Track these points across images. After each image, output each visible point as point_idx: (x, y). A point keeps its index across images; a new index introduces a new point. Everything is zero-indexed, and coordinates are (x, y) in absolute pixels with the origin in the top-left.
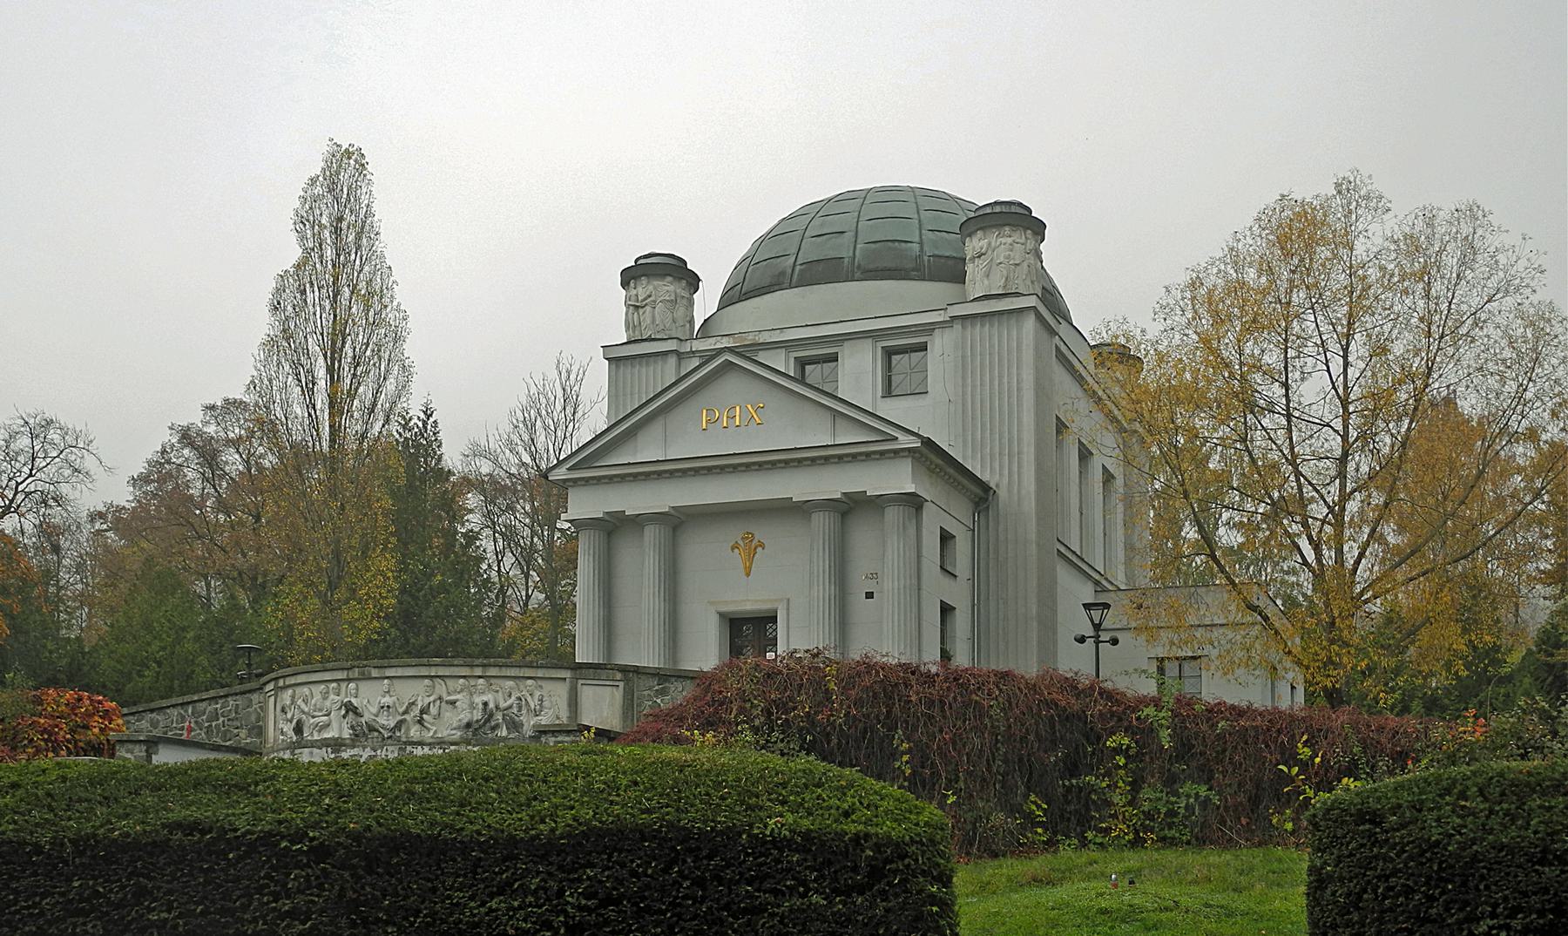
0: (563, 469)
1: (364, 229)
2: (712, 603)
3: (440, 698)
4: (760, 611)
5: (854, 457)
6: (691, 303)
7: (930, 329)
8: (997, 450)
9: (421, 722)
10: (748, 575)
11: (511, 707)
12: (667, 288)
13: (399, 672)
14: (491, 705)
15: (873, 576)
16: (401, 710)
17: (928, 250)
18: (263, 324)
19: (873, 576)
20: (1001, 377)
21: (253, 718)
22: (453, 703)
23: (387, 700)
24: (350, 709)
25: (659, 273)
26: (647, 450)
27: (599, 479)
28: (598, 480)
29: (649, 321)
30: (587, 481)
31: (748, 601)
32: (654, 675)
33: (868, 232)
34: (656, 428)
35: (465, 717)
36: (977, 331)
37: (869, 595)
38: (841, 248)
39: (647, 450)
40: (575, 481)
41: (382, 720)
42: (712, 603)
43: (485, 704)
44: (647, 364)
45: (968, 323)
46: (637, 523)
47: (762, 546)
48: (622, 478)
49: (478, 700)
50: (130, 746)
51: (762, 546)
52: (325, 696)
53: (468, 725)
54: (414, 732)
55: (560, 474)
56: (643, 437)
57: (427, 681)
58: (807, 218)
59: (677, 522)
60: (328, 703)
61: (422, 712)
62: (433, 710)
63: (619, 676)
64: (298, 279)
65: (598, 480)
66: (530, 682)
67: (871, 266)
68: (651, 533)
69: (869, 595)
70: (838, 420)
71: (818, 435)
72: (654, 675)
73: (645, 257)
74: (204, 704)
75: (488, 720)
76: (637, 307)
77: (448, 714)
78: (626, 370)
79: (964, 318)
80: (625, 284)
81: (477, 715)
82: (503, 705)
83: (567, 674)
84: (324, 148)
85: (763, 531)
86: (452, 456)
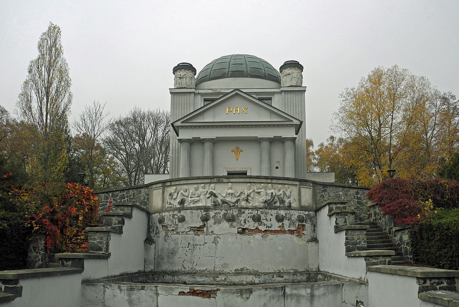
1: (59, 53)
3: (254, 191)
4: (241, 171)
5: (278, 126)
7: (273, 93)
9: (247, 200)
10: (237, 160)
11: (280, 195)
13: (237, 180)
14: (274, 194)
15: (278, 162)
16: (237, 195)
17: (267, 73)
18: (25, 76)
19: (278, 162)
20: (296, 109)
21: (142, 198)
22: (259, 193)
23: (230, 191)
24: (212, 194)
26: (208, 118)
27: (191, 126)
29: (185, 82)
30: (187, 127)
32: (321, 185)
33: (250, 65)
34: (211, 112)
35: (264, 198)
36: (289, 96)
37: (277, 168)
38: (243, 68)
39: (208, 118)
40: (182, 127)
41: (228, 199)
43: (272, 193)
44: (184, 96)
45: (286, 93)
47: (242, 151)
49: (269, 192)
50: (122, 208)
51: (242, 151)
52: (197, 189)
53: (265, 202)
54: (243, 204)
55: (179, 124)
56: (206, 115)
57: (249, 184)
59: (215, 142)
60: (198, 192)
61: (248, 196)
62: (252, 195)
63: (311, 185)
64: (37, 64)
66: (286, 186)
67: (252, 74)
69: (277, 168)
70: (272, 114)
71: (265, 117)
72: (321, 185)
73: (183, 63)
74: (117, 193)
75: (273, 200)
76: (180, 78)
77: (257, 197)
78: (177, 97)
79: (285, 91)
80: (174, 73)
81: (269, 198)
82: (278, 194)
83: (297, 183)
84: (48, 25)
85: (242, 146)
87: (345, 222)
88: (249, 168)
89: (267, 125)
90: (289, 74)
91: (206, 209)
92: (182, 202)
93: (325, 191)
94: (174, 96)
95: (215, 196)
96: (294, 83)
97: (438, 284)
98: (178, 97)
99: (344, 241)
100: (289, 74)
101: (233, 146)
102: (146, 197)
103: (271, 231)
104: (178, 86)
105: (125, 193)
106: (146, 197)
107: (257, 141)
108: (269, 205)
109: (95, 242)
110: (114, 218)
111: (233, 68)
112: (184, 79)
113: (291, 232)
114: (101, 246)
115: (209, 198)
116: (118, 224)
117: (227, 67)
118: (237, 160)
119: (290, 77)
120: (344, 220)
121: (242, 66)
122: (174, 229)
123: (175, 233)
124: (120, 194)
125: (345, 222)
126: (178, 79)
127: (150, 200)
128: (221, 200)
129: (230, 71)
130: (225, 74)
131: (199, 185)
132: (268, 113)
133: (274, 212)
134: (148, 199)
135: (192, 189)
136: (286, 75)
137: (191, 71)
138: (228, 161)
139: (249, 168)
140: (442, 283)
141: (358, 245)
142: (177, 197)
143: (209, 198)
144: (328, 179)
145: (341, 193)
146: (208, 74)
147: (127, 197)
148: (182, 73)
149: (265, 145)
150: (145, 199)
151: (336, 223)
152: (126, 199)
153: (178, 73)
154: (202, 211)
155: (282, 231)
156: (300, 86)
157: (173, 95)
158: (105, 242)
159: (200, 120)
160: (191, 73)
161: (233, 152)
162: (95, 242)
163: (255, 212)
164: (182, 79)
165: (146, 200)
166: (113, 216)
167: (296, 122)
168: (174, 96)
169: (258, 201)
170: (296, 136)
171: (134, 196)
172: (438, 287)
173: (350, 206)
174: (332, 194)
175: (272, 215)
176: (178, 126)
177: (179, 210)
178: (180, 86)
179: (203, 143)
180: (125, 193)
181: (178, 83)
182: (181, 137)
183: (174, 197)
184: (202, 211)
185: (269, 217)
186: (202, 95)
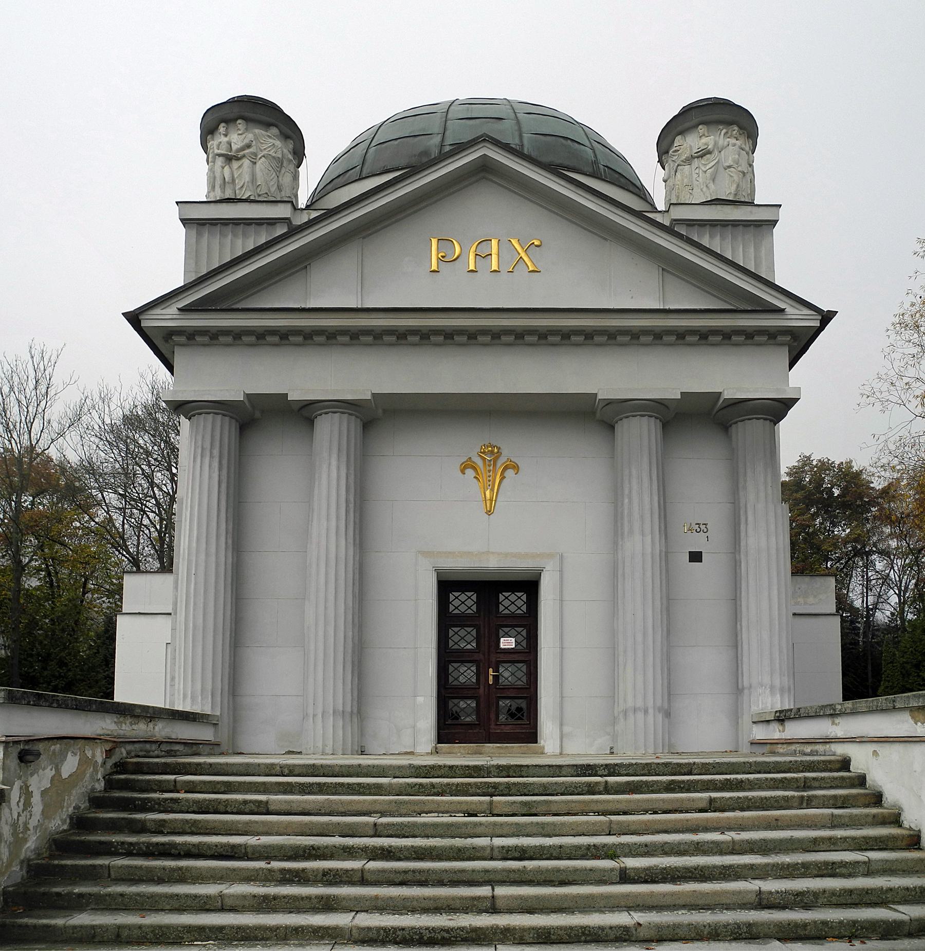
0: (172, 310)
2: (426, 554)
6: (296, 177)
8: (632, 863)
10: (489, 513)
12: (270, 143)
15: (701, 528)
25: (247, 119)
26: (333, 289)
28: (237, 336)
29: (247, 178)
30: (214, 337)
31: (490, 548)
37: (696, 557)
42: (426, 554)
46: (304, 414)
47: (516, 468)
48: (284, 337)
51: (516, 468)
55: (168, 317)
58: (364, 146)
59: (374, 418)
65: (237, 336)
68: (329, 429)
69: (696, 557)
70: (665, 273)
71: (630, 288)
85: (514, 444)
86: (198, 189)
88: (551, 556)
89: (646, 331)
90: (703, 153)
94: (199, 235)
96: (726, 192)
98: (216, 241)
100: (703, 153)
101: (468, 442)
104: (218, 195)
107: (597, 417)
112: (246, 162)
118: (489, 513)
119: (708, 163)
126: (220, 161)
136: (689, 160)
137: (275, 131)
139: (551, 556)
144: (811, 600)
148: (235, 137)
149: (639, 433)
153: (219, 141)
156: (751, 204)
157: (194, 232)
159: (287, 296)
160: (278, 143)
161: (470, 473)
164: (235, 164)
167: (796, 318)
168: (199, 235)
178: (229, 194)
179: (310, 422)
181: (218, 182)
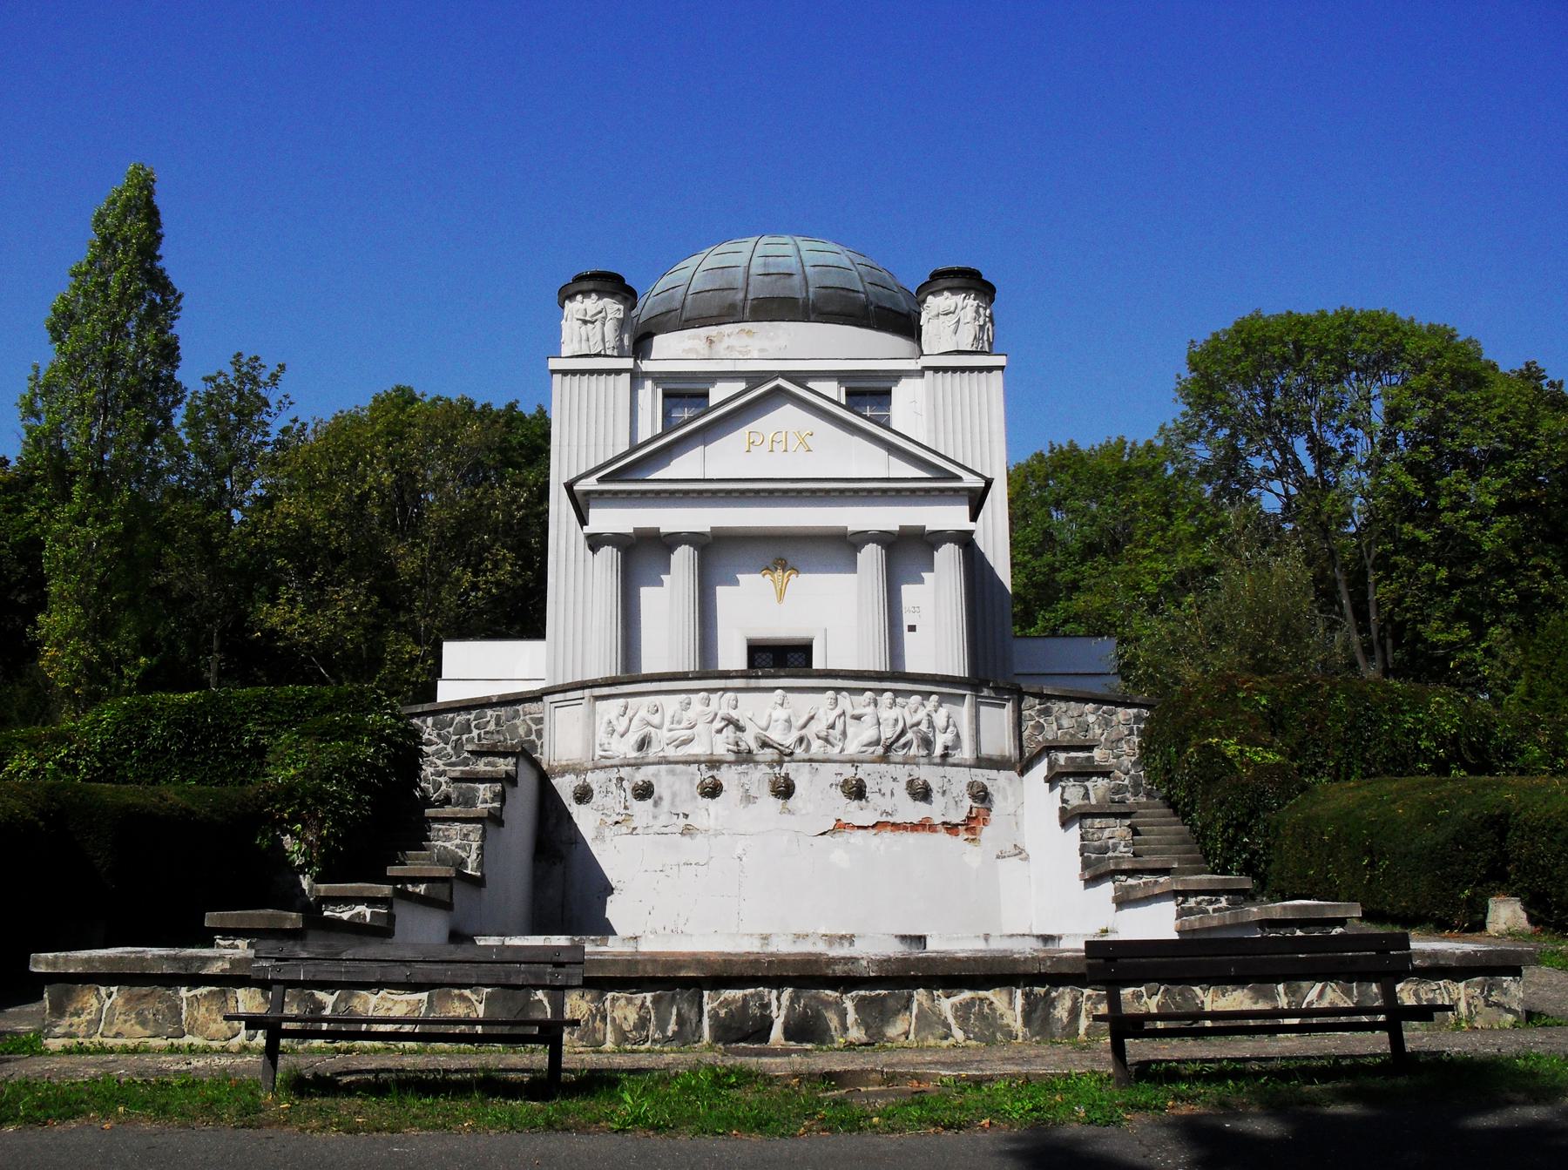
7: (897, 376)
21: (522, 731)
22: (858, 718)
35: (869, 734)
39: (685, 467)
40: (602, 493)
54: (817, 747)
55: (590, 484)
71: (869, 463)
79: (936, 369)
87: (1086, 796)
91: (714, 764)
92: (643, 744)
93: (1046, 712)
95: (740, 728)
97: (1211, 903)
99: (1077, 843)
102: (534, 728)
103: (893, 824)
105: (472, 717)
106: (534, 728)
108: (886, 752)
109: (447, 844)
110: (482, 787)
111: (758, 290)
113: (951, 828)
114: (464, 855)
115: (720, 731)
116: (493, 801)
117: (740, 283)
120: (1082, 791)
121: (788, 281)
122: (619, 818)
123: (624, 830)
124: (458, 719)
125: (1086, 796)
127: (545, 734)
128: (756, 738)
129: (750, 296)
130: (733, 306)
131: (693, 697)
132: (882, 453)
133: (902, 773)
134: (539, 734)
135: (671, 704)
138: (754, 607)
140: (1217, 901)
141: (1110, 854)
142: (627, 730)
143: (720, 731)
145: (1091, 719)
146: (677, 304)
147: (477, 727)
150: (529, 732)
151: (1064, 801)
152: (475, 733)
154: (703, 766)
155: (925, 826)
158: (475, 845)
162: (447, 844)
163: (848, 772)
165: (533, 737)
166: (482, 781)
169: (858, 739)
170: (969, 526)
171: (497, 724)
172: (1210, 908)
173: (1118, 757)
174: (1065, 722)
175: (895, 780)
176: (588, 493)
177: (637, 765)
180: (472, 717)
182: (591, 528)
183: (621, 729)
184: (703, 766)
185: (887, 785)
186: (658, 378)
